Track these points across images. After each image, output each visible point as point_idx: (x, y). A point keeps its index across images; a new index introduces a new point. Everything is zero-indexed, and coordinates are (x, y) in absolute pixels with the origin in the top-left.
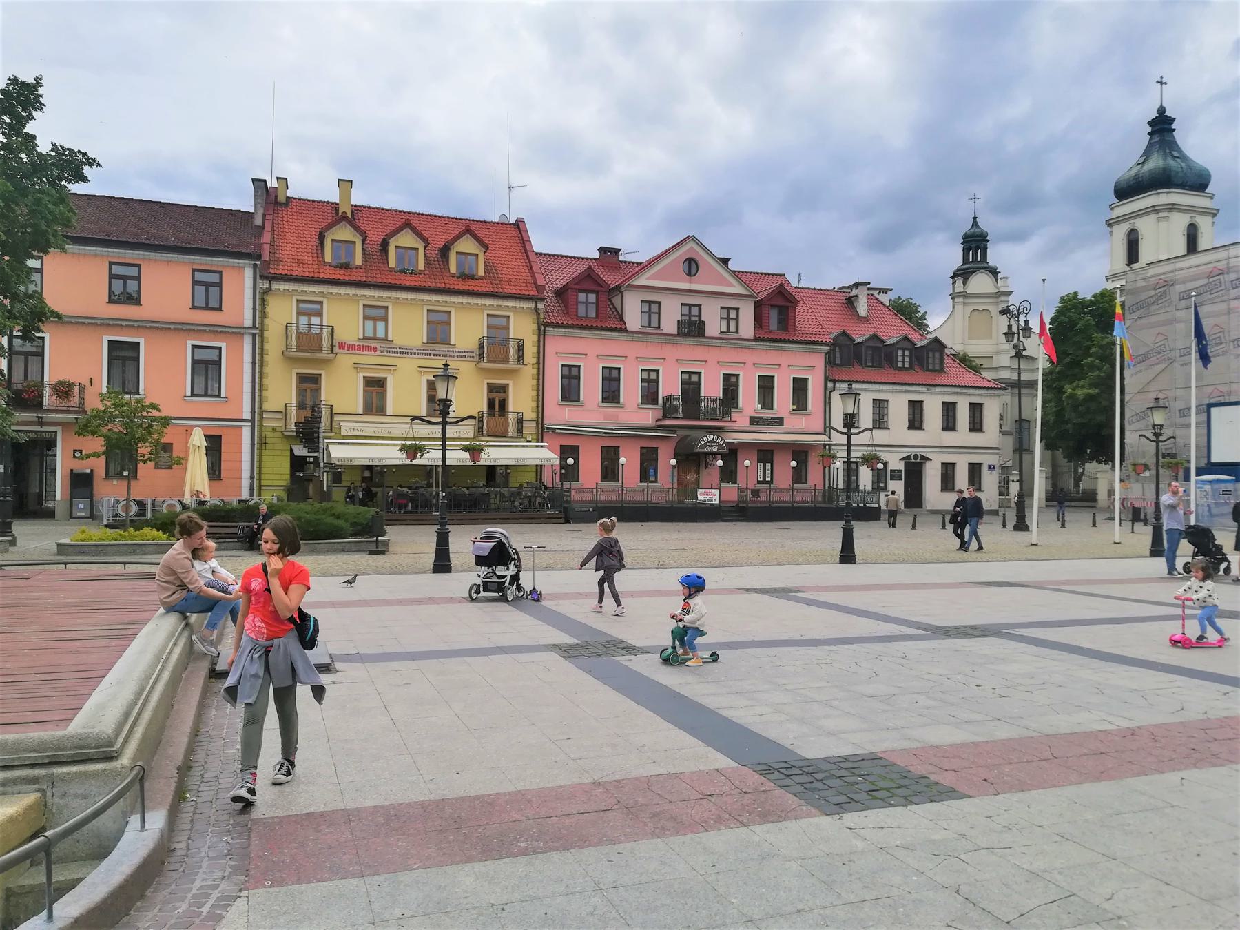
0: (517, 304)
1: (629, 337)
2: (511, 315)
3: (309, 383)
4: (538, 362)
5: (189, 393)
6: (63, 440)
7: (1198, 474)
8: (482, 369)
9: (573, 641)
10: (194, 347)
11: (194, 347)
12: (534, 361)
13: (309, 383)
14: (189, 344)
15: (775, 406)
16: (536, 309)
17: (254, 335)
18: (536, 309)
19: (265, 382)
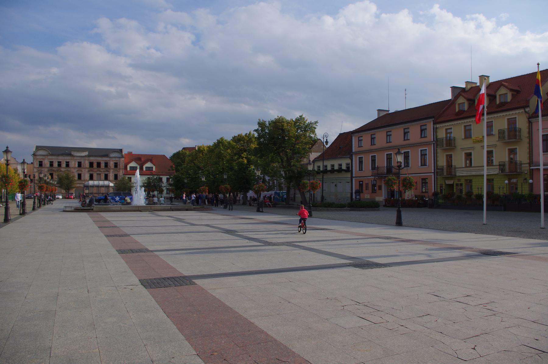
0: (517, 111)
1: (94, 212)
2: (517, 116)
3: (449, 158)
4: (529, 136)
5: (420, 165)
6: (545, 217)
7: (539, 170)
8: (506, 143)
9: (319, 154)
10: (421, 150)
11: (421, 150)
12: (527, 135)
13: (449, 158)
14: (386, 153)
15: (445, 156)
16: (525, 112)
17: (434, 144)
18: (525, 112)
19: (438, 159)
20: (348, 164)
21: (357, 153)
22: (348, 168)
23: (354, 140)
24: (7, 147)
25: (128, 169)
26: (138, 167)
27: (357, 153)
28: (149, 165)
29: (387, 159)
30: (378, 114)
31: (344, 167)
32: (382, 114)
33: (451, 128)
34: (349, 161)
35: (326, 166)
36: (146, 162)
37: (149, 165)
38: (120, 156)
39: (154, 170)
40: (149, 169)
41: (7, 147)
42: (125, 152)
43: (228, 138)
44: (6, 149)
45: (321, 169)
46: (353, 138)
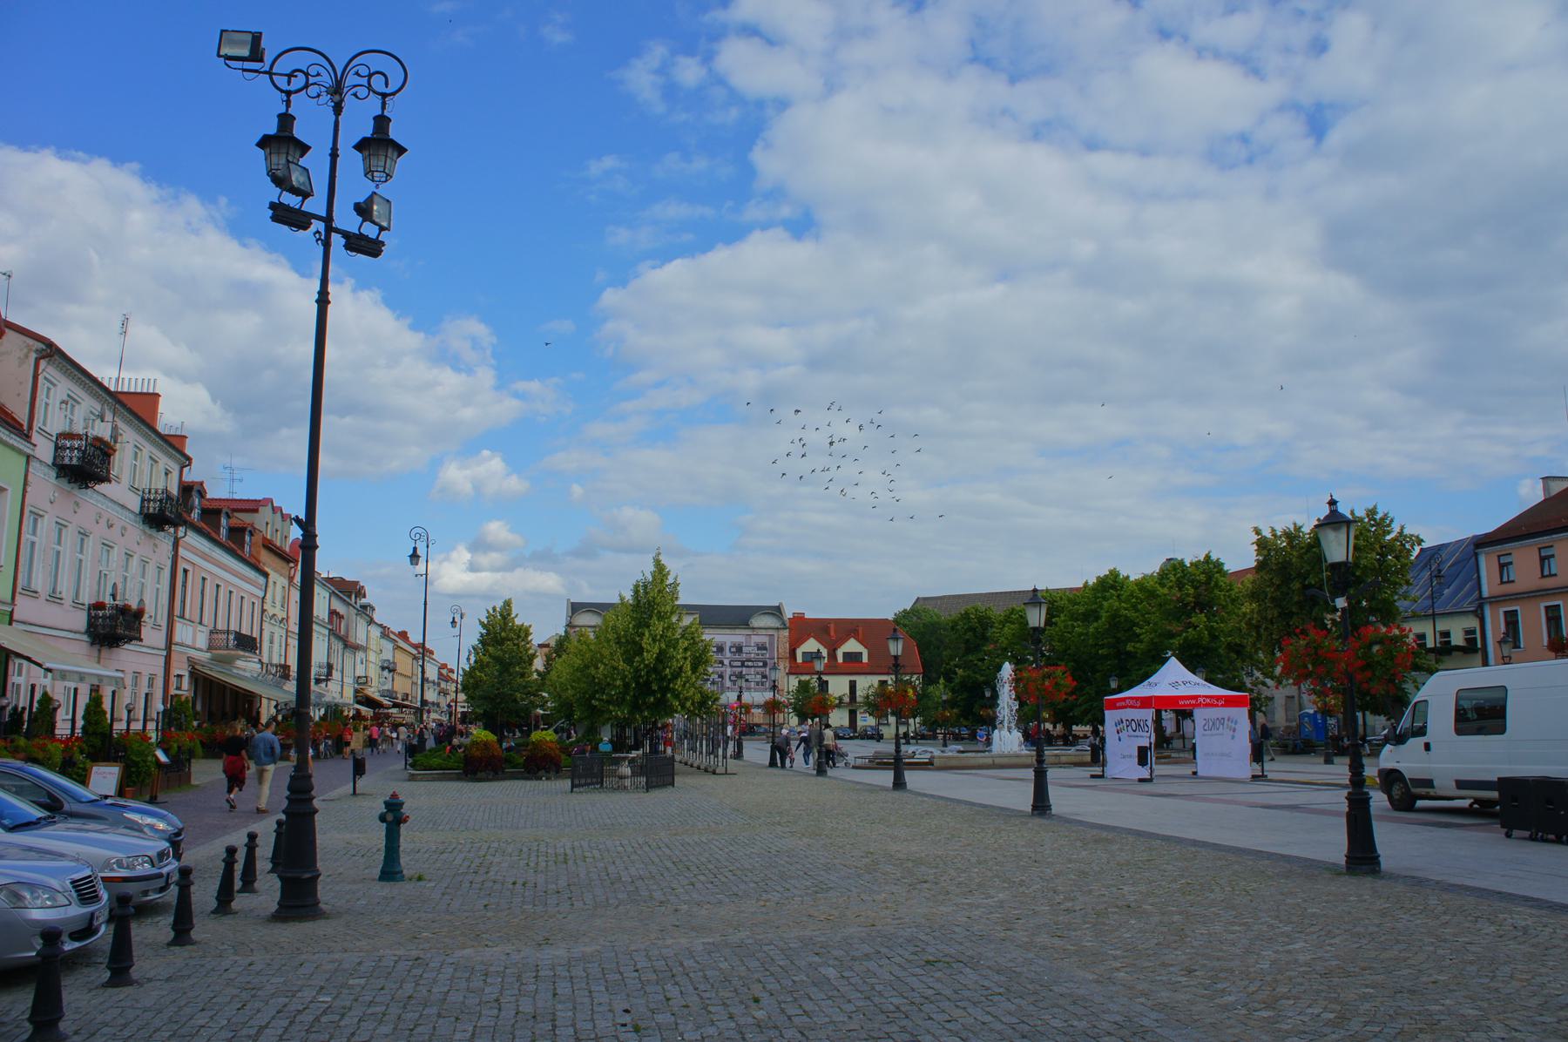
14: (1543, 605)
20: (1468, 632)
21: (1496, 600)
22: (1471, 642)
23: (1487, 565)
24: (1332, 503)
25: (840, 660)
26: (824, 652)
27: (1496, 600)
28: (852, 646)
29: (1549, 619)
30: (1546, 489)
31: (1457, 639)
32: (1557, 487)
33: (33, 687)
34: (1473, 623)
35: (1446, 634)
36: (843, 641)
37: (852, 646)
38: (777, 624)
39: (865, 659)
40: (852, 657)
41: (1332, 503)
42: (788, 614)
43: (1139, 567)
44: (1326, 511)
45: (1430, 644)
46: (1482, 560)
